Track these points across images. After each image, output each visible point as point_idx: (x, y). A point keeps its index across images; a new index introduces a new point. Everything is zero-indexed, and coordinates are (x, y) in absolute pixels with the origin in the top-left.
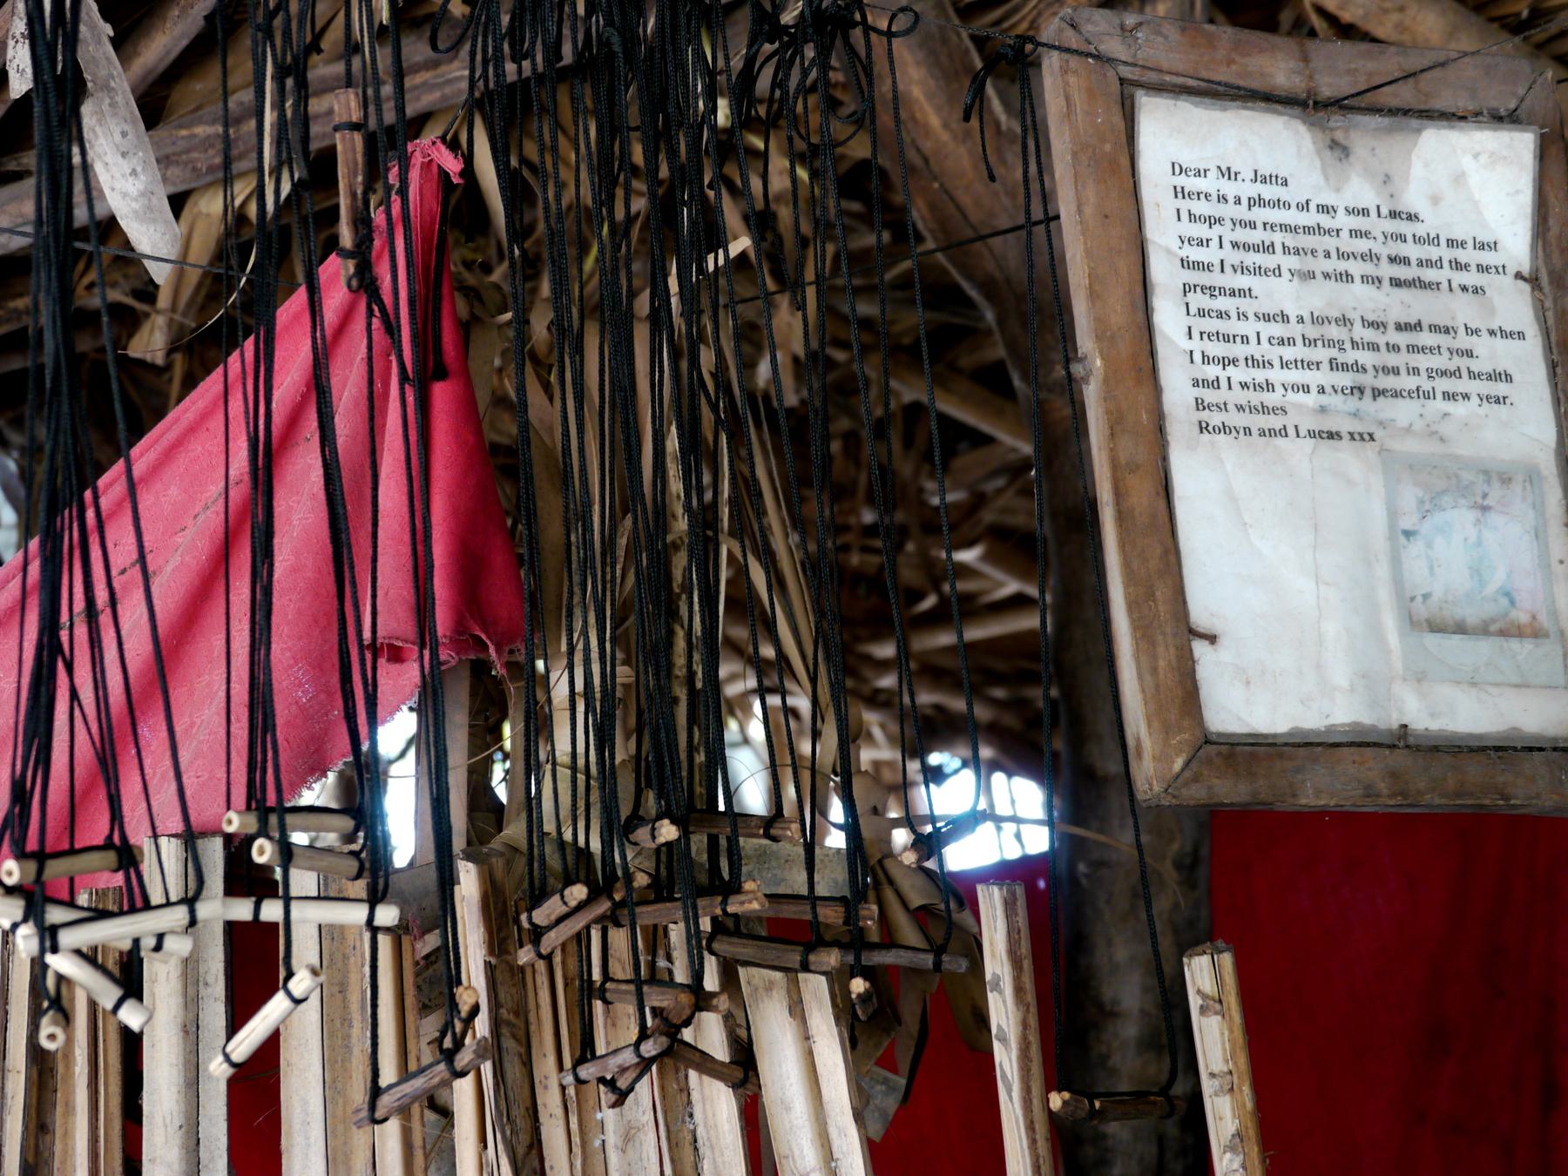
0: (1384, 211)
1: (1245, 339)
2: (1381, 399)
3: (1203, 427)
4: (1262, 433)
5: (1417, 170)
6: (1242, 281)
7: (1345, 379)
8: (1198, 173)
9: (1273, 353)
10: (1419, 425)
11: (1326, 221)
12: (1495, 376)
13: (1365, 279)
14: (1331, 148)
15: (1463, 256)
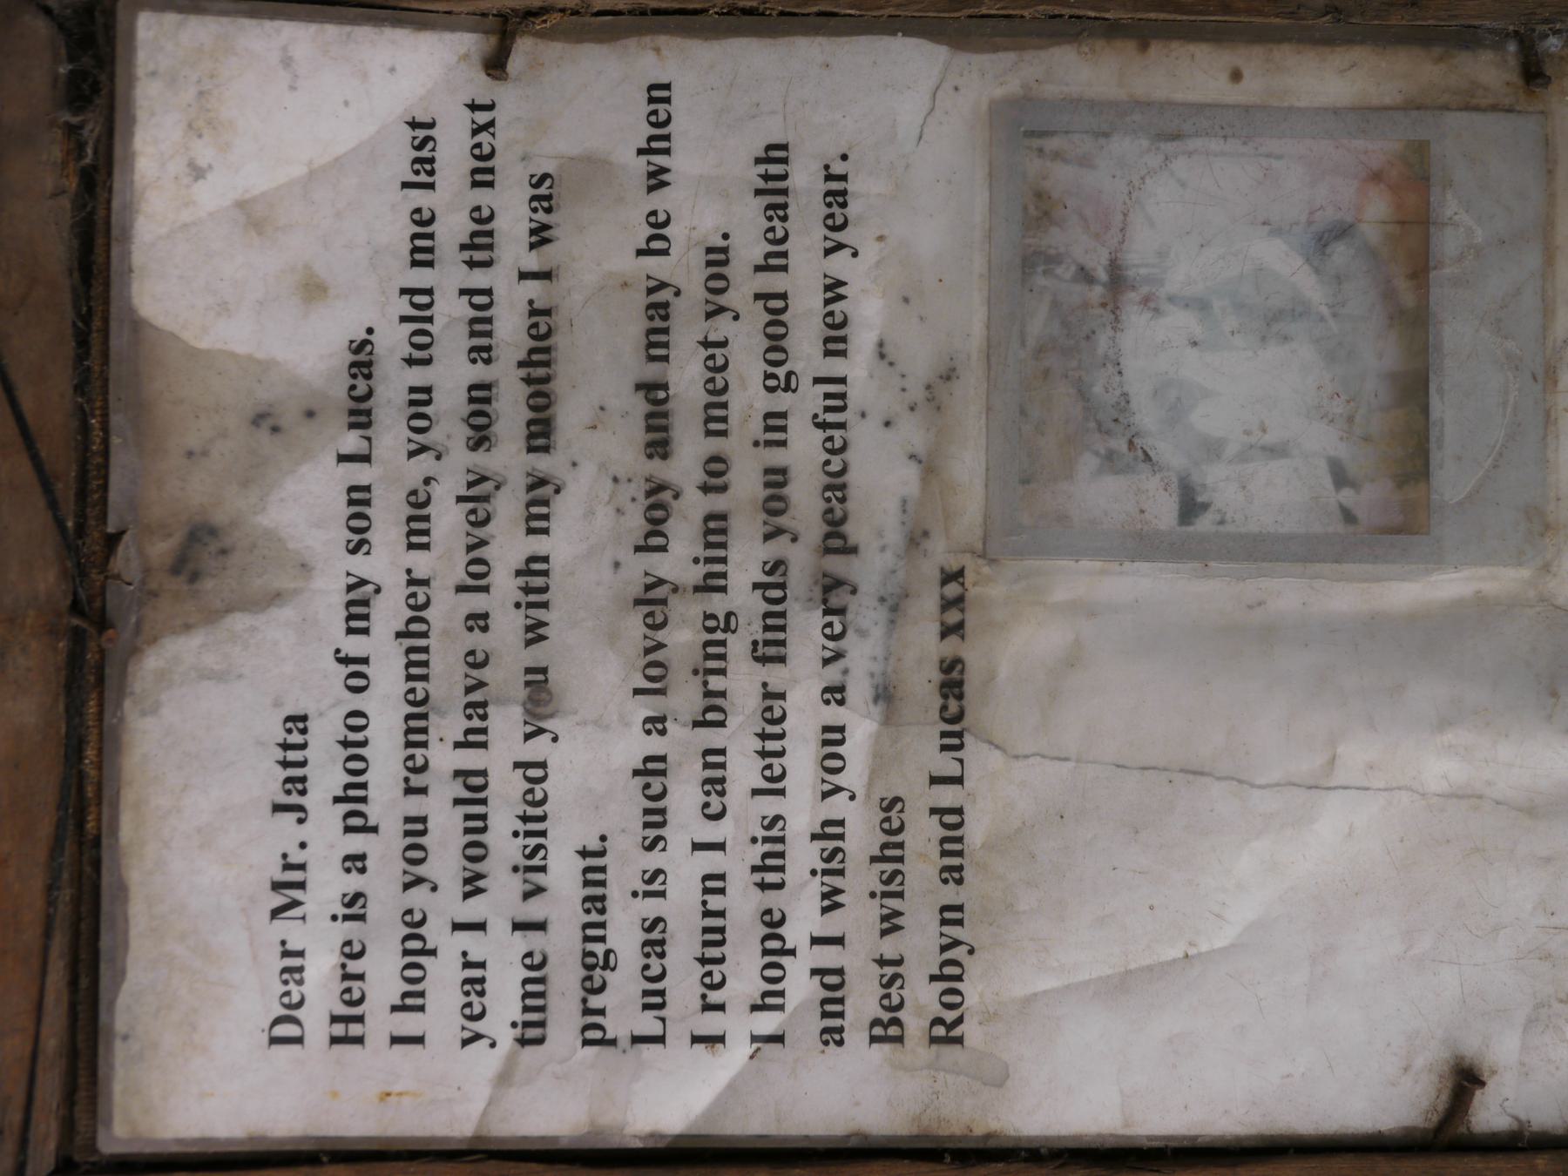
0: (351, 442)
1: (714, 883)
2: (855, 531)
3: (946, 1033)
4: (953, 874)
5: (235, 335)
6: (563, 872)
7: (806, 629)
8: (293, 973)
9: (744, 814)
10: (912, 433)
11: (389, 613)
12: (774, 194)
13: (536, 524)
14: (194, 577)
15: (452, 228)
